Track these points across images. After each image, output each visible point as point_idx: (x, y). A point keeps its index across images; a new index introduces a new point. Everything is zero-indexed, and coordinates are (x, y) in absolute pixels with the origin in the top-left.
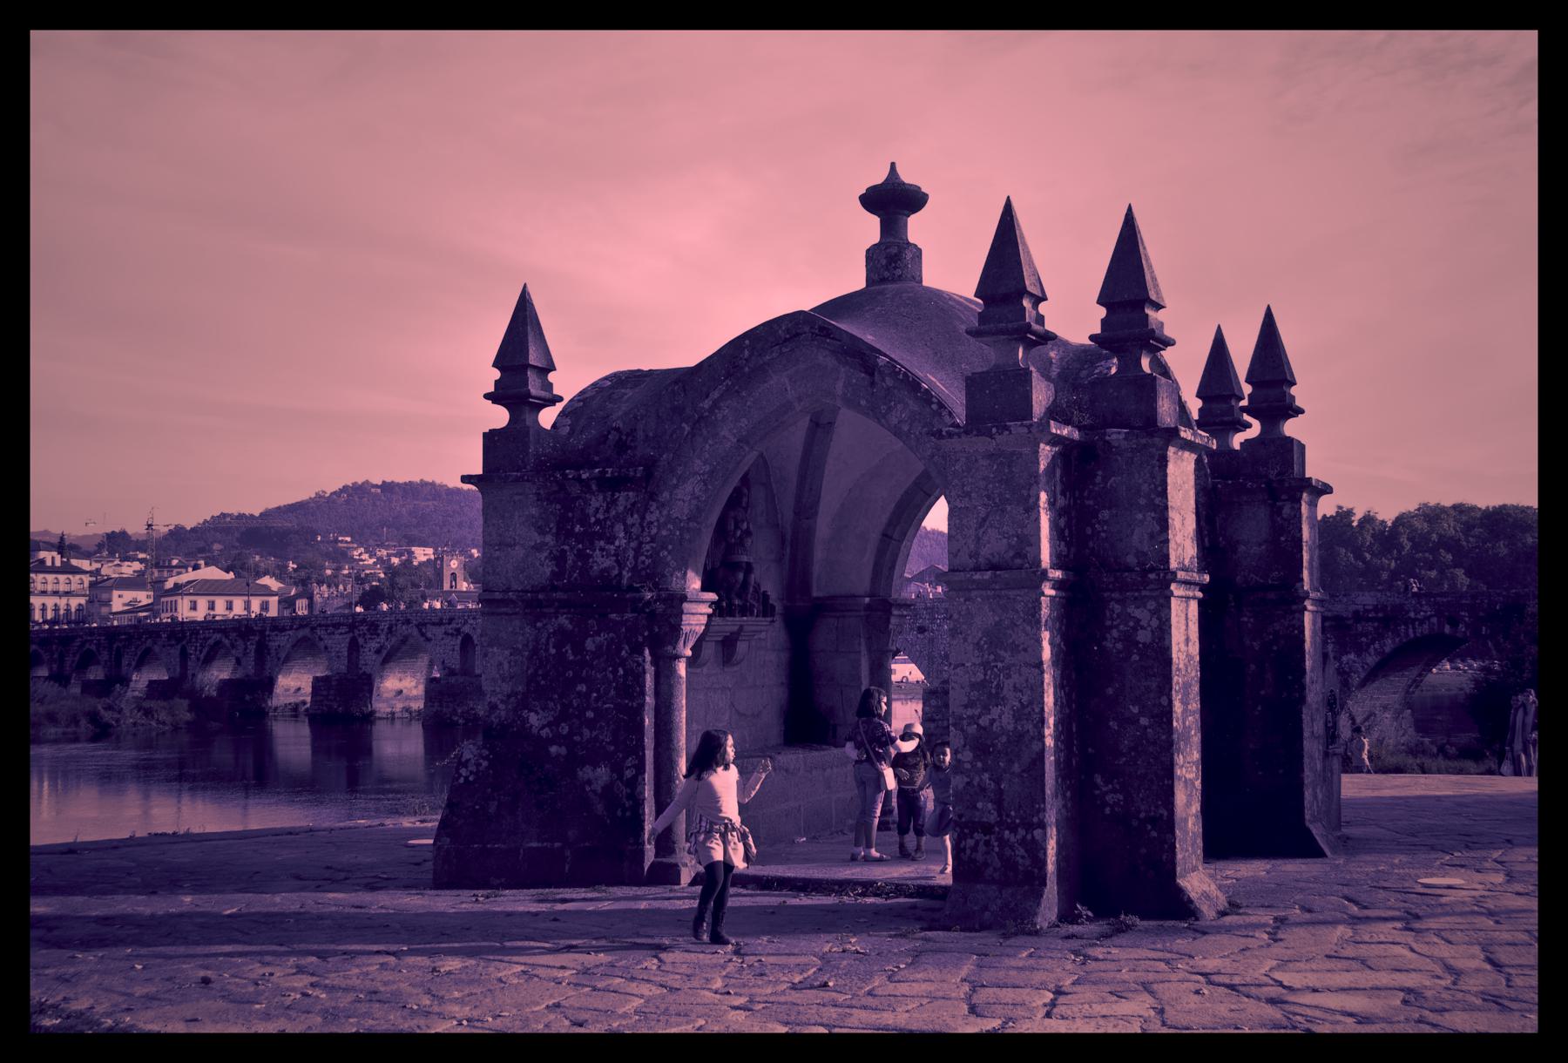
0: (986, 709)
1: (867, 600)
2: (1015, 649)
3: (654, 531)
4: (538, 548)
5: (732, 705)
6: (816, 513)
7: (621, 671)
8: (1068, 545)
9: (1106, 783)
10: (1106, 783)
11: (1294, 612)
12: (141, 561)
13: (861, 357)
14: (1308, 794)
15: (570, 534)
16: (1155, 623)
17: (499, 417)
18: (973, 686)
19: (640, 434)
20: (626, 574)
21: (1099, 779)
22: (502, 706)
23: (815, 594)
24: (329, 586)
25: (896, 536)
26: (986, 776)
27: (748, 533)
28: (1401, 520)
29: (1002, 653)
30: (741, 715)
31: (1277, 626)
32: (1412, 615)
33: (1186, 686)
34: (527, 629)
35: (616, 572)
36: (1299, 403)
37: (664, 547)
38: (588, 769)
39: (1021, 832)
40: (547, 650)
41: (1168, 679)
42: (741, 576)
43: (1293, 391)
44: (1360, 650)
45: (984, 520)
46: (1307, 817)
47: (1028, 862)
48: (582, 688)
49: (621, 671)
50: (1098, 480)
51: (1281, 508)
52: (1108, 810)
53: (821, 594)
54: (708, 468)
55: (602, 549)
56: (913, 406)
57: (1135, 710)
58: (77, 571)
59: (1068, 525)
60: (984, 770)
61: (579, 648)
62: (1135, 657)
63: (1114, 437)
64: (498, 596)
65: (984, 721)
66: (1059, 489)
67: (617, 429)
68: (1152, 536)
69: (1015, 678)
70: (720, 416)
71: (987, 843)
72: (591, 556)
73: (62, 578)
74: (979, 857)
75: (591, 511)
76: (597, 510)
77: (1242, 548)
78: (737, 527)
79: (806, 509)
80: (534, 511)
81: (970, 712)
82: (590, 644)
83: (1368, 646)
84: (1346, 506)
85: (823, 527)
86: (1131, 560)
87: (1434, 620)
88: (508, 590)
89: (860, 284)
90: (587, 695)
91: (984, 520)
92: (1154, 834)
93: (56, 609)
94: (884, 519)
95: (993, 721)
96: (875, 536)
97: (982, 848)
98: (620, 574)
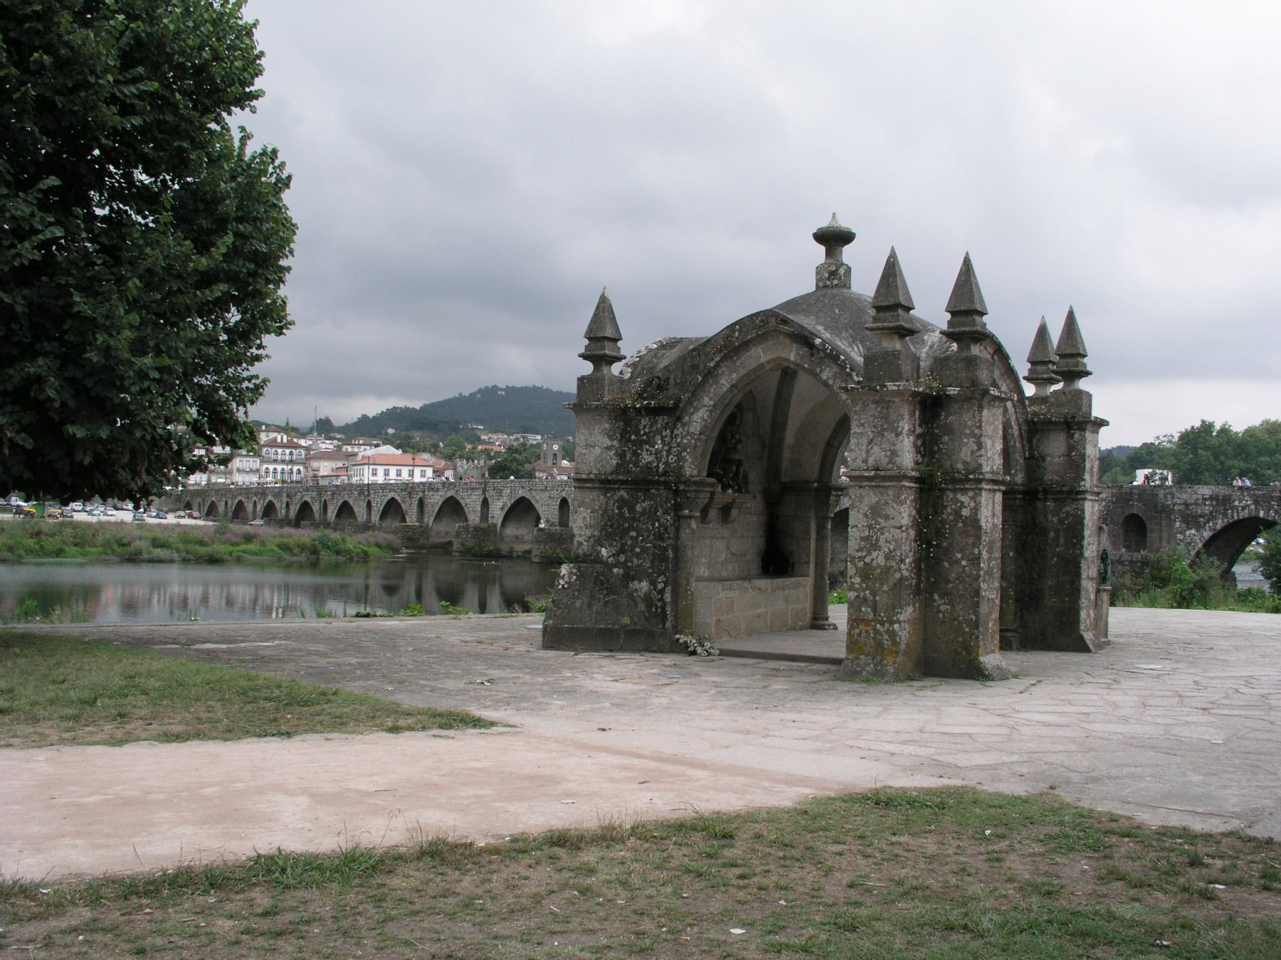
0: (869, 553)
1: (816, 485)
2: (887, 517)
3: (679, 440)
4: (608, 448)
5: (728, 548)
6: (785, 429)
7: (657, 525)
8: (923, 456)
9: (941, 599)
10: (941, 599)
11: (1078, 499)
12: (339, 440)
13: (804, 339)
14: (1083, 614)
15: (629, 440)
16: (972, 504)
17: (587, 368)
18: (862, 539)
19: (672, 381)
20: (662, 466)
21: (936, 597)
22: (585, 544)
23: (783, 480)
24: (468, 461)
25: (835, 445)
26: (868, 592)
27: (739, 441)
28: (1250, 432)
29: (880, 520)
30: (733, 554)
31: (1068, 509)
32: (1237, 503)
33: (991, 543)
34: (602, 497)
35: (655, 464)
36: (1089, 368)
37: (685, 450)
38: (636, 582)
39: (887, 625)
40: (613, 510)
41: (979, 538)
42: (734, 468)
43: (1086, 360)
44: (1199, 527)
45: (872, 440)
46: (1082, 628)
47: (890, 643)
48: (633, 534)
49: (657, 525)
50: (942, 417)
51: (1073, 435)
52: (941, 615)
53: (786, 480)
54: (712, 403)
55: (647, 450)
56: (835, 369)
57: (959, 556)
58: (297, 446)
59: (923, 444)
60: (867, 588)
61: (632, 509)
62: (961, 525)
63: (951, 393)
64: (584, 476)
65: (868, 560)
66: (917, 422)
67: (658, 378)
68: (972, 452)
69: (887, 535)
70: (720, 372)
71: (867, 631)
72: (640, 454)
73: (288, 451)
74: (862, 639)
75: (641, 427)
76: (645, 426)
77: (1049, 459)
78: (732, 438)
79: (778, 426)
80: (607, 426)
81: (859, 554)
82: (638, 508)
83: (1205, 524)
84: (1209, 419)
85: (790, 437)
86: (960, 466)
87: (1253, 507)
88: (591, 473)
89: (811, 287)
90: (636, 538)
91: (872, 440)
92: (967, 630)
93: (283, 472)
94: (829, 433)
95: (873, 560)
96: (822, 445)
97: (864, 634)
98: (658, 466)
